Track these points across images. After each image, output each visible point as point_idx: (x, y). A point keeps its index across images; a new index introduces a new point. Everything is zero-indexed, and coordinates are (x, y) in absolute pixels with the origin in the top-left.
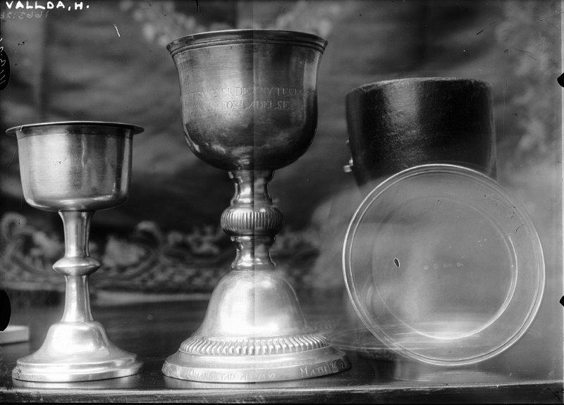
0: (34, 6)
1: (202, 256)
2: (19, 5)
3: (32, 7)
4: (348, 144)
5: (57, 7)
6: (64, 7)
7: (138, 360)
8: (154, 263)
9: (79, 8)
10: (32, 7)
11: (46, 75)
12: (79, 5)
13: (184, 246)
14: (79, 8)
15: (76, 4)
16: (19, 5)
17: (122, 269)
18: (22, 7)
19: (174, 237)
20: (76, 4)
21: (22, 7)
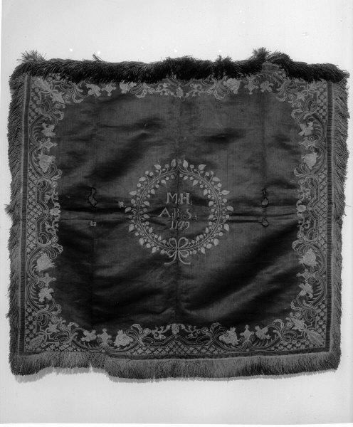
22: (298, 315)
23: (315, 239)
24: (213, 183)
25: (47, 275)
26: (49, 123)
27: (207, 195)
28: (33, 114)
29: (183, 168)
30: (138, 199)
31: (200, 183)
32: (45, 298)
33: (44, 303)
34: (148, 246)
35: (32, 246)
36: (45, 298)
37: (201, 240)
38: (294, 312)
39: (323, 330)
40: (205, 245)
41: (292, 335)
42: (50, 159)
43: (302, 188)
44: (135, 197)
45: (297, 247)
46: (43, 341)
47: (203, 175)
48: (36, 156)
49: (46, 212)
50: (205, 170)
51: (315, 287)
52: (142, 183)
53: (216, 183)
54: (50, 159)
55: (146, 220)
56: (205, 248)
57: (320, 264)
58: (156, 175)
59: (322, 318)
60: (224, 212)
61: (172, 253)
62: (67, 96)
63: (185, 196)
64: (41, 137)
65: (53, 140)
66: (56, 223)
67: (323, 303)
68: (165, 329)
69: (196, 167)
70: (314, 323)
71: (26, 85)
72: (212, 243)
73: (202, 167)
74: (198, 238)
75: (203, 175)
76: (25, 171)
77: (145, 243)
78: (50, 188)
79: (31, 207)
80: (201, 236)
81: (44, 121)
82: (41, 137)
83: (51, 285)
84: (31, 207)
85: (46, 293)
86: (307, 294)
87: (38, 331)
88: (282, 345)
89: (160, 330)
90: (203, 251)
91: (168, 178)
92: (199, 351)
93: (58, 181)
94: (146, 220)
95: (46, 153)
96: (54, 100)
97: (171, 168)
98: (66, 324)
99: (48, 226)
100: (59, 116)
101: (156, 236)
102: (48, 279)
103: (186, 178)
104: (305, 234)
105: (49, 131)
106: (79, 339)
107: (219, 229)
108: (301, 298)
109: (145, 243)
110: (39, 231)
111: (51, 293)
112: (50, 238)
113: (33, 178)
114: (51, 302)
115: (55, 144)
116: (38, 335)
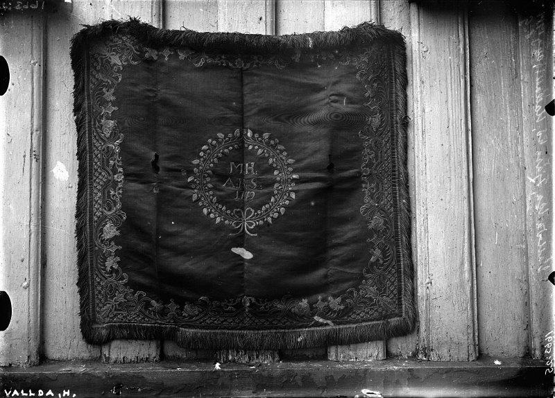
0: (29, 394)
1: (228, 312)
2: (16, 392)
3: (26, 394)
4: (283, 362)
5: (47, 395)
6: (53, 395)
7: (285, 45)
8: (206, 315)
9: (66, 395)
10: (26, 394)
11: (158, 231)
12: (66, 393)
13: (220, 307)
14: (66, 395)
15: (64, 391)
16: (16, 392)
17: (191, 317)
18: (18, 394)
19: (216, 303)
20: (64, 391)
21: (18, 394)
22: (370, 281)
23: (382, 203)
24: (278, 151)
25: (113, 243)
26: (109, 87)
27: (272, 164)
28: (94, 80)
29: (248, 138)
30: (201, 168)
31: (265, 151)
32: (111, 267)
33: (111, 273)
34: (212, 216)
35: (98, 214)
36: (111, 267)
37: (266, 210)
38: (367, 279)
39: (395, 295)
40: (271, 215)
41: (365, 303)
42: (111, 123)
43: (367, 150)
44: (198, 166)
45: (365, 213)
46: (111, 310)
47: (268, 144)
48: (99, 122)
49: (110, 178)
50: (270, 138)
51: (384, 252)
52: (205, 151)
53: (281, 151)
54: (111, 123)
55: (210, 189)
56: (272, 218)
57: (388, 228)
58: (219, 143)
59: (393, 283)
60: (289, 180)
61: (237, 224)
62: (124, 58)
63: (250, 165)
64: (104, 103)
65: (114, 104)
66: (119, 189)
67: (393, 267)
68: (234, 302)
69: (261, 136)
70: (385, 290)
71: (88, 226)
72: (279, 212)
73: (266, 135)
74: (263, 208)
75: (268, 144)
76: (90, 138)
77: (209, 213)
78: (113, 154)
79: (97, 174)
80: (267, 206)
81: (104, 86)
82: (104, 103)
83: (117, 253)
84: (97, 174)
85: (111, 263)
86: (378, 260)
87: (106, 300)
88: (355, 313)
89: (229, 302)
90: (270, 220)
91: (231, 148)
92: (271, 323)
93: (120, 145)
94: (210, 189)
95: (108, 118)
96: (112, 63)
97: (234, 137)
98: (133, 294)
99: (112, 193)
100: (117, 78)
101: (220, 206)
102: (113, 248)
103: (251, 147)
104: (372, 198)
105: (109, 96)
106: (146, 308)
107: (285, 197)
108: (372, 264)
109: (209, 213)
110: (104, 198)
111: (118, 262)
112: (115, 205)
113: (97, 144)
114: (117, 271)
115: (116, 108)
116: (106, 305)
